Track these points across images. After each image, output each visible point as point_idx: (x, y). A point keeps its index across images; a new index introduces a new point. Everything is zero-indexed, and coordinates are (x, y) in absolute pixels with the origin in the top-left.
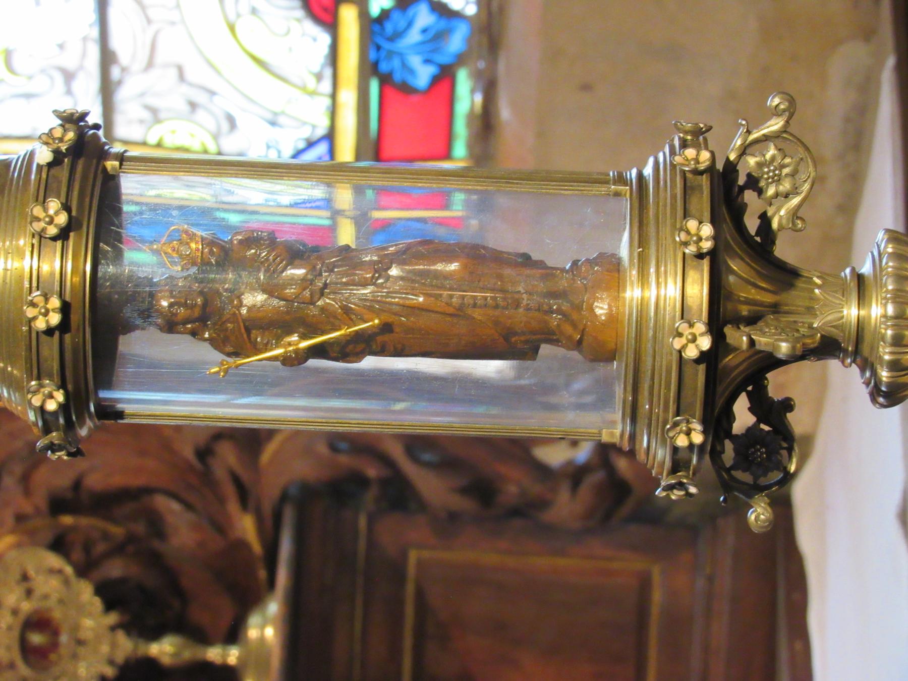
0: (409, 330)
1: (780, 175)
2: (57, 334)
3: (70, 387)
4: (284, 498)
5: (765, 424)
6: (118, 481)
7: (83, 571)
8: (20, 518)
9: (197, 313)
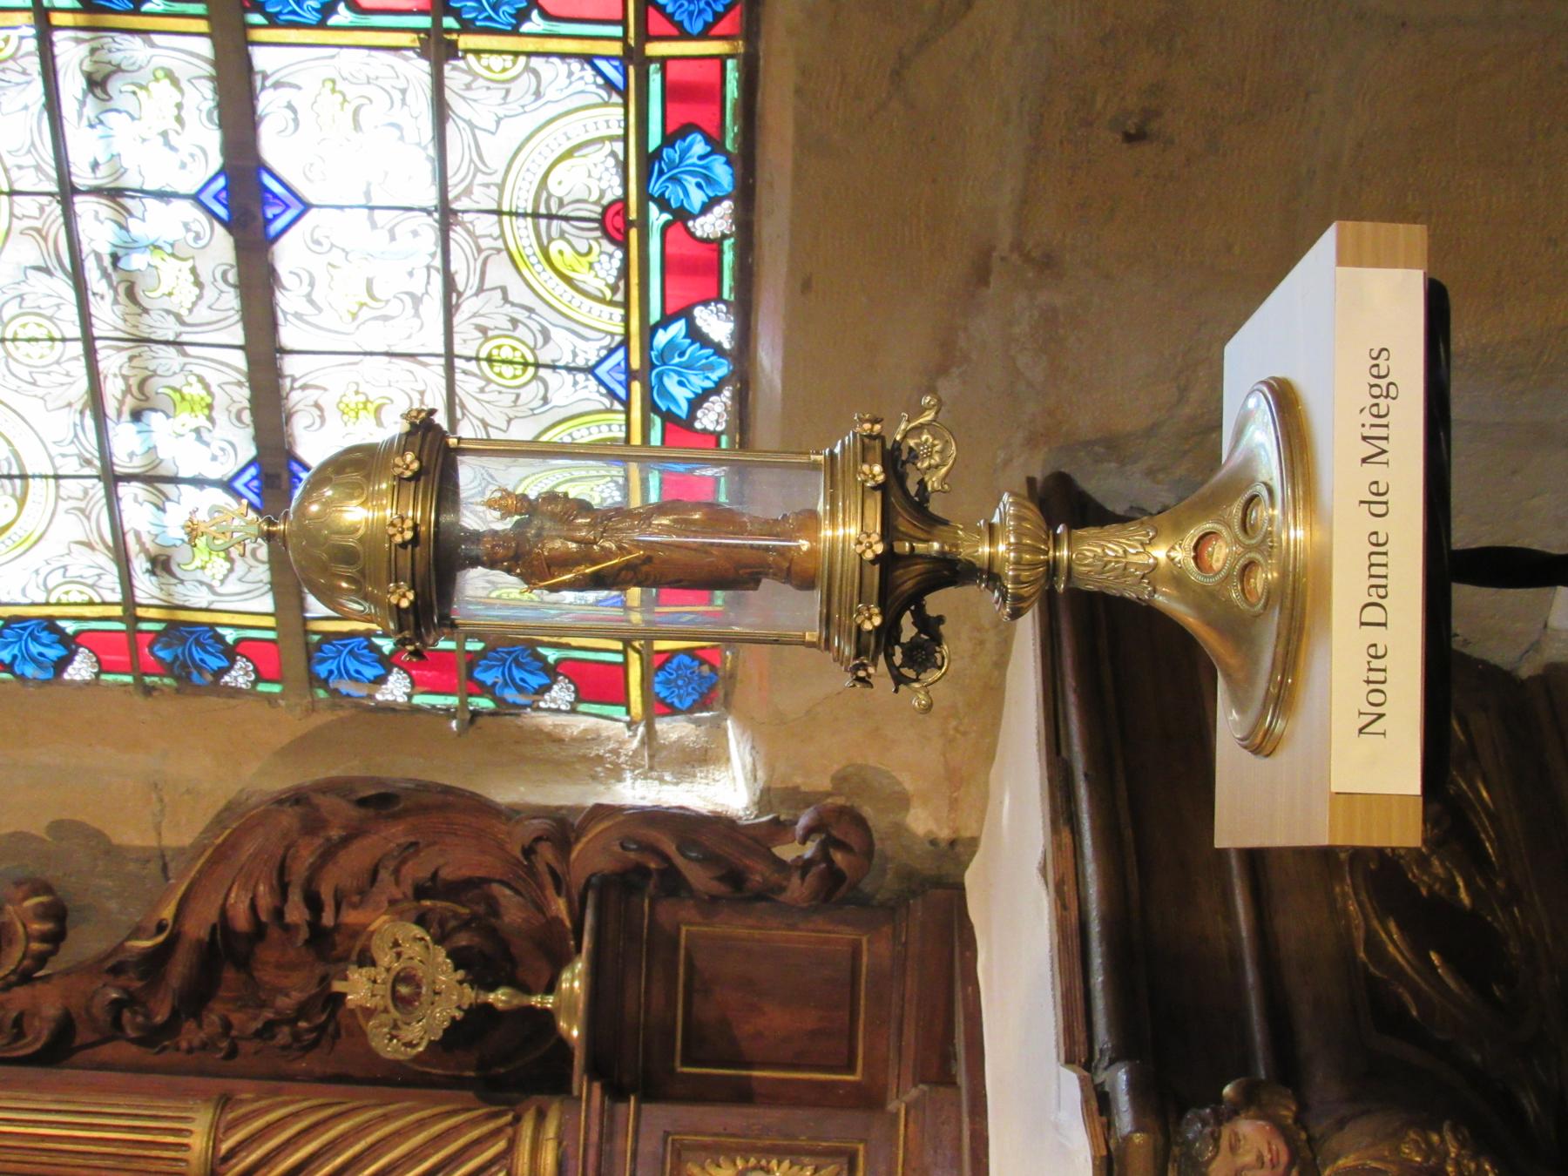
0: (664, 561)
1: (931, 452)
2: (410, 547)
3: (419, 589)
4: (588, 885)
5: (925, 634)
6: (466, 872)
7: (440, 940)
8: (393, 902)
9: (511, 553)
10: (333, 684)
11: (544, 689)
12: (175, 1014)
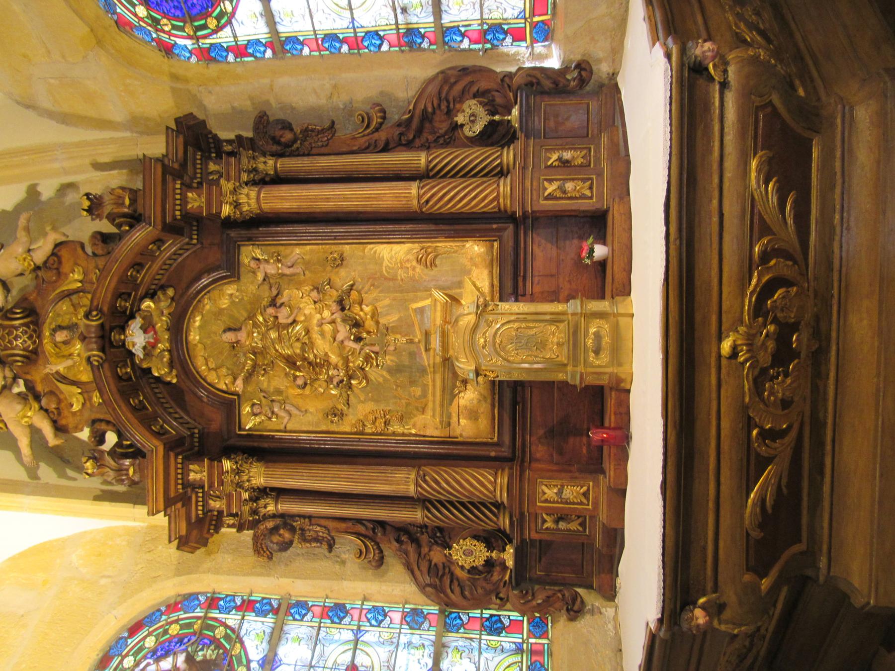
10: (449, 44)
11: (504, 39)
12: (414, 137)
